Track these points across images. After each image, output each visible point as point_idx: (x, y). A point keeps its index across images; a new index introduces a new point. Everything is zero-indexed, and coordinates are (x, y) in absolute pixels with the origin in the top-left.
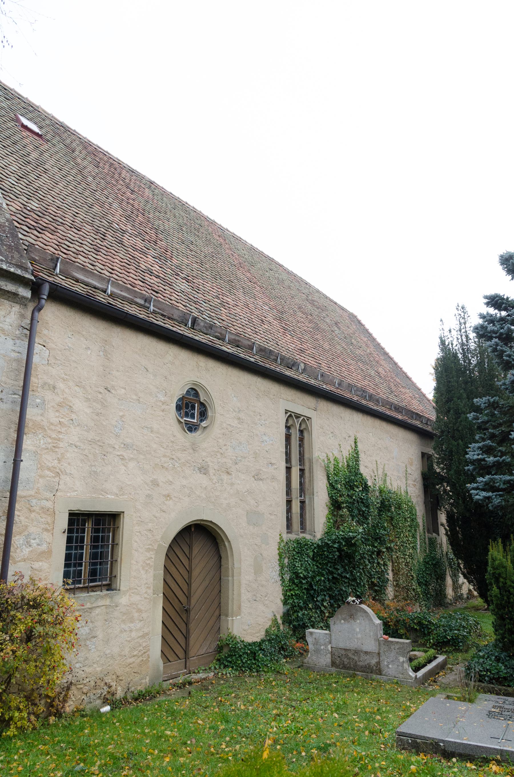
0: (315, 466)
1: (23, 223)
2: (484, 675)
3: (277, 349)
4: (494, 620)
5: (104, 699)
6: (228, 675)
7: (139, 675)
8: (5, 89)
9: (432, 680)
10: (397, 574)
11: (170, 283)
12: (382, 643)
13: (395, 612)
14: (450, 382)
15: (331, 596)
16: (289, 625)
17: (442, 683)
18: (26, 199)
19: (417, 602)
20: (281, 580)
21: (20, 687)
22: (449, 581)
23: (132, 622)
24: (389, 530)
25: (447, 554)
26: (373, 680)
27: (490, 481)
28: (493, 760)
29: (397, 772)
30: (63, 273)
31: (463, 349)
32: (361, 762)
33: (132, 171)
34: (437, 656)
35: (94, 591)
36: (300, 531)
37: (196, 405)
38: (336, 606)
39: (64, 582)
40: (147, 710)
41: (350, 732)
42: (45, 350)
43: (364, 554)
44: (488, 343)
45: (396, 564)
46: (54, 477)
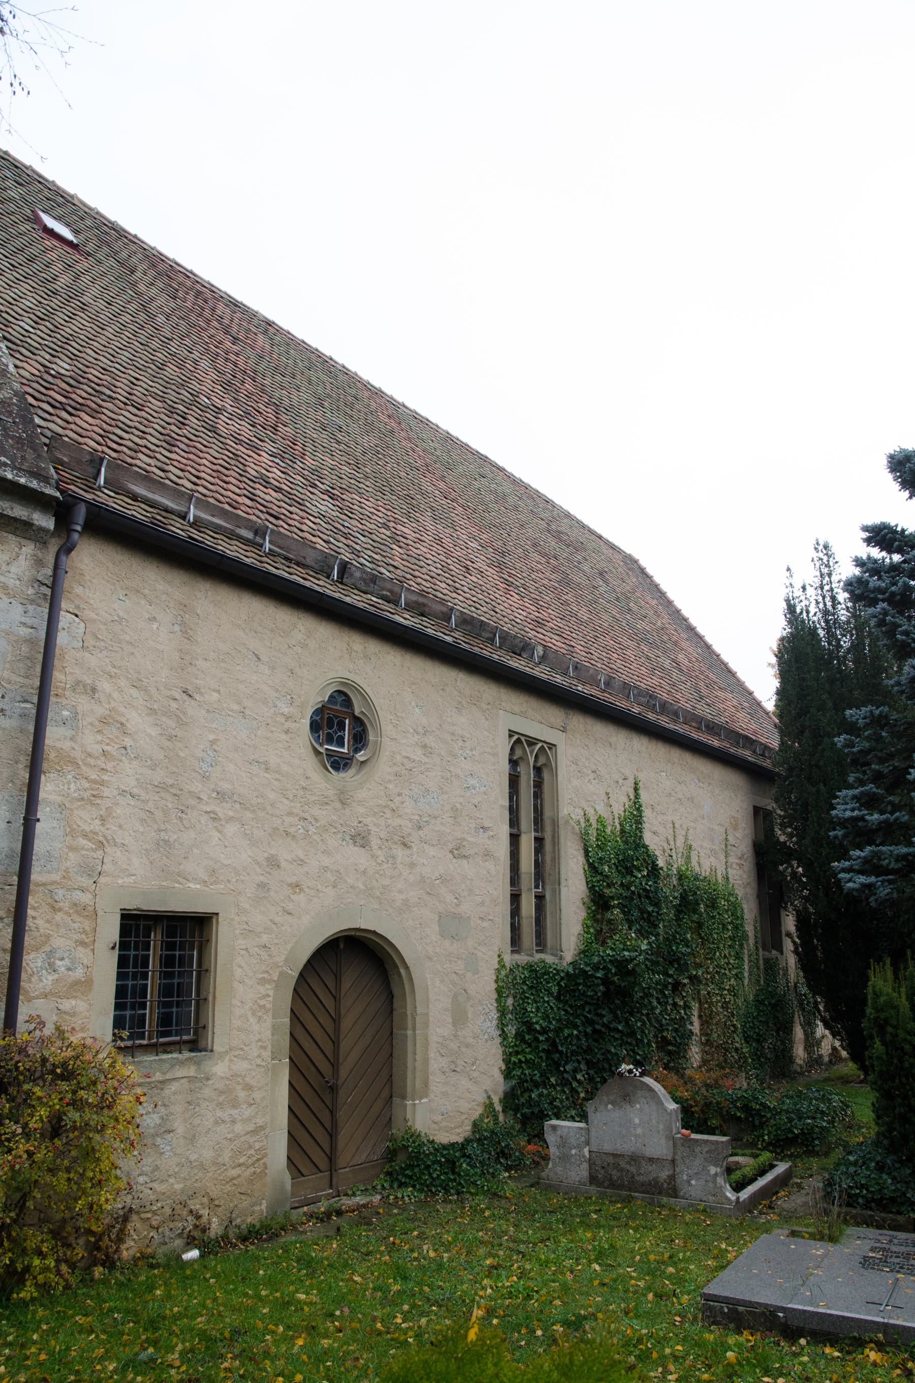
0: (562, 833)
1: (43, 398)
2: (856, 1195)
3: (494, 619)
4: (875, 1100)
5: (188, 1238)
6: (406, 1199)
7: (248, 1199)
8: (17, 167)
9: (765, 1205)
10: (707, 1022)
11: (301, 501)
12: (679, 1143)
13: (703, 1090)
14: (804, 679)
15: (589, 1064)
16: (516, 1114)
17: (783, 1210)
18: (48, 357)
19: (741, 1071)
20: (500, 1035)
21: (42, 1216)
22: (799, 1033)
23: (234, 1107)
24: (694, 946)
25: (796, 986)
26: (662, 1206)
27: (873, 857)
28: (871, 1341)
29: (703, 1362)
30: (110, 484)
31: (827, 622)
32: (641, 1347)
33: (235, 304)
34: (775, 1163)
35: (168, 1053)
36: (535, 948)
37: (347, 722)
38: (599, 1079)
39: (114, 1034)
40: (264, 1258)
41: (621, 1294)
42: (78, 623)
43: (649, 988)
44: (871, 610)
45: (706, 1006)
46: (94, 850)
